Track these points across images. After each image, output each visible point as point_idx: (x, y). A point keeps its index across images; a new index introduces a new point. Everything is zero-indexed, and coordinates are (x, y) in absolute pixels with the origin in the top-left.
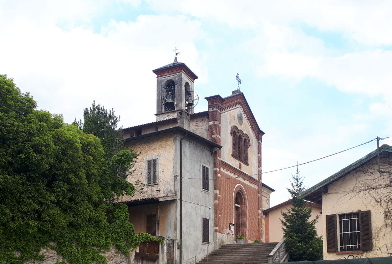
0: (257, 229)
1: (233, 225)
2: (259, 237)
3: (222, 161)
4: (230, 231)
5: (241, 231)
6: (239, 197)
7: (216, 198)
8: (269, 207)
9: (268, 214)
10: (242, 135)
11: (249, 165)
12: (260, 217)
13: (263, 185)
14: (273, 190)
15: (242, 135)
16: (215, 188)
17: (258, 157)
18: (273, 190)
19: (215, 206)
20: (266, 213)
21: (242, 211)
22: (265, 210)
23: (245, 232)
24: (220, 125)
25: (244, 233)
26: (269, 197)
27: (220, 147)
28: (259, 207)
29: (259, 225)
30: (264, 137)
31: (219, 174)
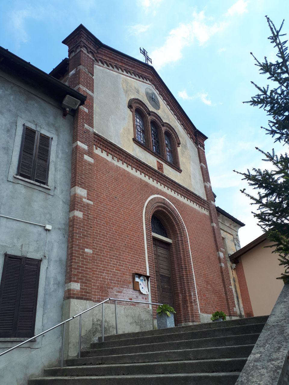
0: (220, 287)
1: (148, 277)
2: (228, 304)
3: (95, 134)
4: (137, 293)
5: (181, 295)
6: (162, 220)
7: (73, 203)
8: (239, 246)
9: (239, 261)
10: (154, 118)
11: (130, 107)
12: (223, 265)
13: (219, 211)
14: (242, 225)
15: (154, 118)
16: (74, 181)
17: (202, 168)
18: (242, 225)
19: (72, 223)
20: (237, 258)
21: (178, 251)
22: (233, 253)
23: (190, 296)
24: (94, 77)
25: (188, 298)
26: (237, 235)
27: (83, 99)
28: (217, 246)
29: (223, 280)
30: (206, 142)
31: (85, 155)
